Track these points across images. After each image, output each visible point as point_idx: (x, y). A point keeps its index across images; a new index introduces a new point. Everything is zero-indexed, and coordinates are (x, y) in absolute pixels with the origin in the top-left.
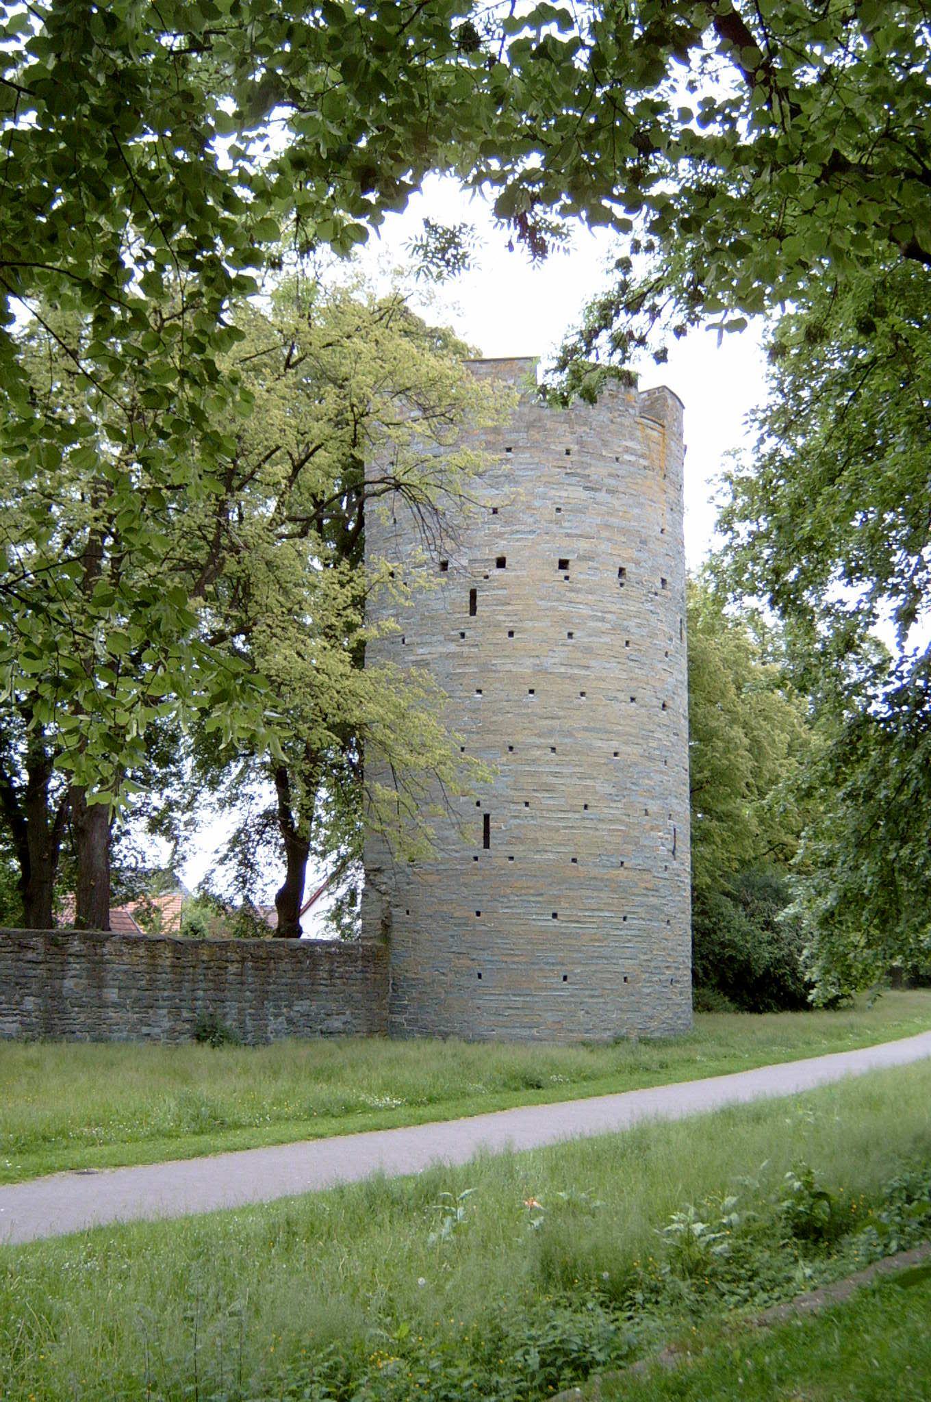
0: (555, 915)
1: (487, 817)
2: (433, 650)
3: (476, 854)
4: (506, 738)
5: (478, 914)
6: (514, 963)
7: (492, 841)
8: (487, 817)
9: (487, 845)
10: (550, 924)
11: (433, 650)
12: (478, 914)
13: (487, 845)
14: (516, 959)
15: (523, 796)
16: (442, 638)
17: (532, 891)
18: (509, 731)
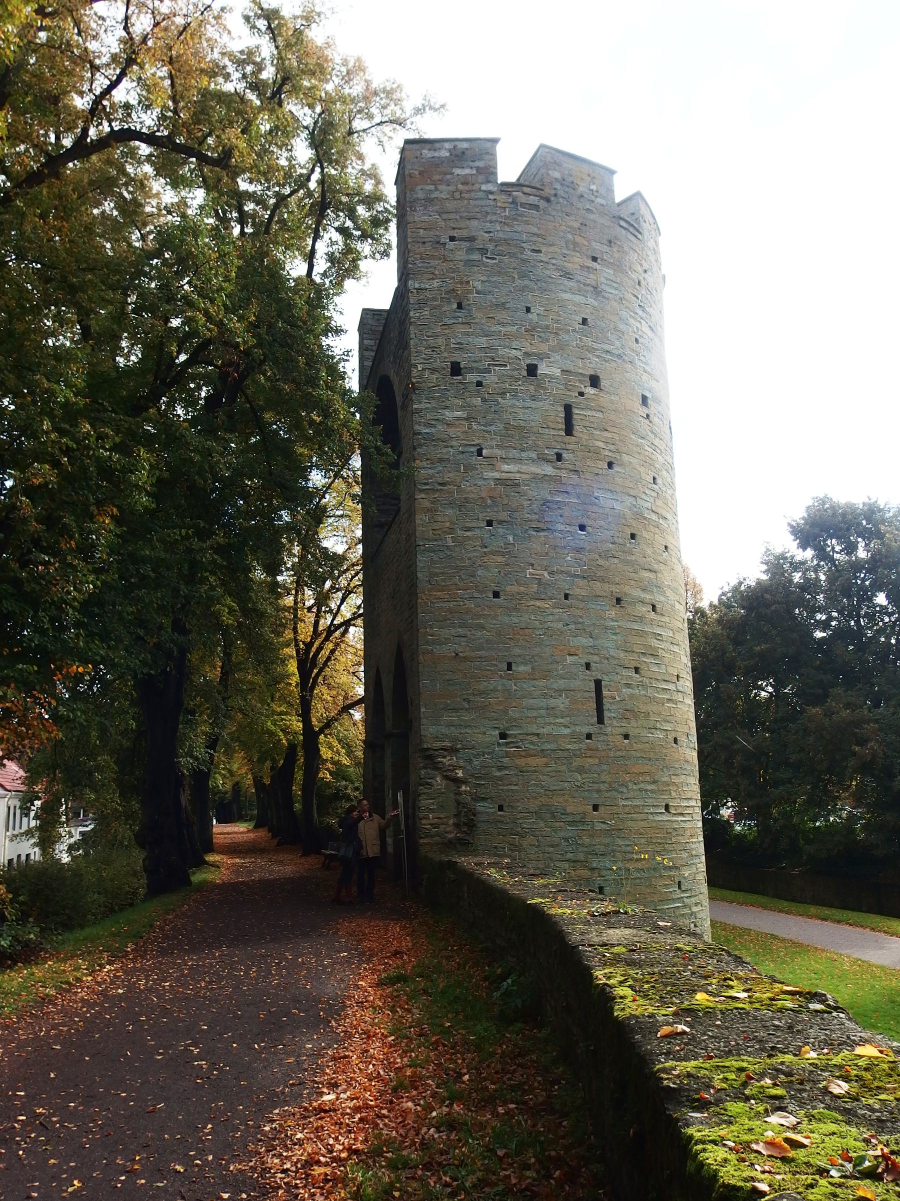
0: (667, 807)
1: (598, 684)
2: (524, 468)
3: (586, 730)
4: (614, 588)
5: (596, 808)
7: (606, 714)
8: (598, 684)
10: (665, 818)
11: (524, 468)
12: (596, 808)
13: (601, 720)
15: (631, 660)
16: (534, 455)
18: (617, 579)
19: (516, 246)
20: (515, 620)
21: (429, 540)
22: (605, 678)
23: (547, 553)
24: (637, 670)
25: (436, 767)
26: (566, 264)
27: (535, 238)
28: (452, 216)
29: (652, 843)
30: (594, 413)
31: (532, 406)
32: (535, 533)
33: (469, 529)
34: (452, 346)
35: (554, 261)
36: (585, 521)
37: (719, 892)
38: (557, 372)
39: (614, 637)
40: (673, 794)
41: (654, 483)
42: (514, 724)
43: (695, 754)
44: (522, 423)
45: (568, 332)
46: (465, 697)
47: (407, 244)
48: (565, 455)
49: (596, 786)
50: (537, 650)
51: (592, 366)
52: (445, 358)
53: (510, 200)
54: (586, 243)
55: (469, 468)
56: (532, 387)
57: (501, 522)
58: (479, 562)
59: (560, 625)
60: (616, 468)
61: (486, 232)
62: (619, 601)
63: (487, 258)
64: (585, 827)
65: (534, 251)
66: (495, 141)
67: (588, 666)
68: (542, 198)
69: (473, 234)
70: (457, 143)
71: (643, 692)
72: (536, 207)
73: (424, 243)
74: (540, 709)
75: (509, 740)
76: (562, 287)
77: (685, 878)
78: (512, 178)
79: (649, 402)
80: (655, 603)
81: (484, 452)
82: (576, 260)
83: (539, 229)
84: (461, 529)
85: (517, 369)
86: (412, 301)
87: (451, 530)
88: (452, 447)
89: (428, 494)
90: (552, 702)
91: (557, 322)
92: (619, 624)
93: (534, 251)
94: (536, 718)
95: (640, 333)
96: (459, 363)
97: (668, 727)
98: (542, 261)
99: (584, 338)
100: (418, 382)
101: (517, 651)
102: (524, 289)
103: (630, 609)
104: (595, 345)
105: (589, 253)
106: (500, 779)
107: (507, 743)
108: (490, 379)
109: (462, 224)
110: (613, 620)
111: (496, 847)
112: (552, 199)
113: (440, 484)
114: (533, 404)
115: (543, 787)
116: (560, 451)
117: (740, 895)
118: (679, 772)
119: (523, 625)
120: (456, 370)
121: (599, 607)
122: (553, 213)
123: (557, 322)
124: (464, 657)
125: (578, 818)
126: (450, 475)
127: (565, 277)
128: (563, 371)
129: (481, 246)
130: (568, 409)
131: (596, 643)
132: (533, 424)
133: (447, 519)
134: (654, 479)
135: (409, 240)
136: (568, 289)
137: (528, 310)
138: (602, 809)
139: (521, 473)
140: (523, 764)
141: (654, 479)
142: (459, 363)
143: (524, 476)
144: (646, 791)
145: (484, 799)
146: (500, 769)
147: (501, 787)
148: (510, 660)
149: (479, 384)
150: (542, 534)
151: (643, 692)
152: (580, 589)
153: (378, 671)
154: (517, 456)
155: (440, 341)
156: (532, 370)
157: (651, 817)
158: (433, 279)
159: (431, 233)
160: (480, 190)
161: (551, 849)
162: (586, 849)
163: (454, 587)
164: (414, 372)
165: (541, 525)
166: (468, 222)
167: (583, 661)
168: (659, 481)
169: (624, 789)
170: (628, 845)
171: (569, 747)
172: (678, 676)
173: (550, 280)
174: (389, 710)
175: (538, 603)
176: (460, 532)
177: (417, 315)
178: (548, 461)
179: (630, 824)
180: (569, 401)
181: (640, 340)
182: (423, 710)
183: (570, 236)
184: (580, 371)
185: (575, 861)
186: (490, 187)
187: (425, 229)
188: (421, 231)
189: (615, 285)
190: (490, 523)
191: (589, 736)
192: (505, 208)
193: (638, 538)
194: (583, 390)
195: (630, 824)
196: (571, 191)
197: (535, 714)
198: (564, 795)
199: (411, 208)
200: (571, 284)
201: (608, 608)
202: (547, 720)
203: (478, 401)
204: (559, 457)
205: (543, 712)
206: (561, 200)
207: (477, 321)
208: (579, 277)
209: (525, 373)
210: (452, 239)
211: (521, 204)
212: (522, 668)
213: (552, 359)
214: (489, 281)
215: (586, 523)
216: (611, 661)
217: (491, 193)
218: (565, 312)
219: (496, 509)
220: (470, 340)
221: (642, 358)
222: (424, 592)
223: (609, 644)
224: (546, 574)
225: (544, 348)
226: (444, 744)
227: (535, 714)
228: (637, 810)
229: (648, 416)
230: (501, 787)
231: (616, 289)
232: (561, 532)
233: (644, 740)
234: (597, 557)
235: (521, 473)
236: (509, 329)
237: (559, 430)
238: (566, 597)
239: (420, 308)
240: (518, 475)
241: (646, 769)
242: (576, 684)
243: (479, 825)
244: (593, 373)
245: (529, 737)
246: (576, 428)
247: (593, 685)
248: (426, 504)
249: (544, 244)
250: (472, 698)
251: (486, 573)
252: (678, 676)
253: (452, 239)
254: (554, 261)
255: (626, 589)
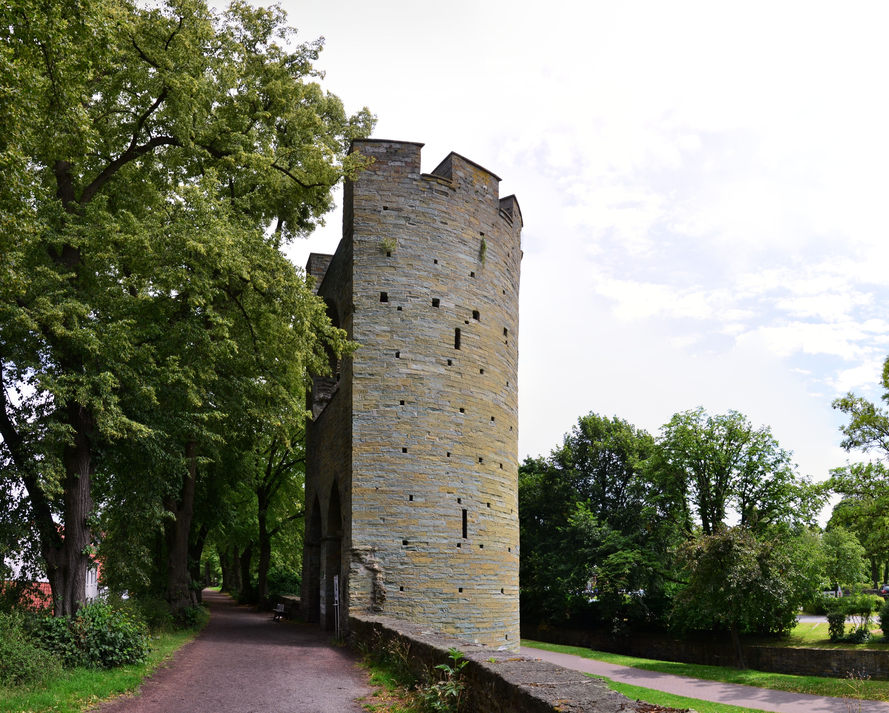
0: (502, 591)
1: (465, 512)
2: (426, 368)
3: (459, 541)
4: (478, 451)
5: (461, 590)
6: (483, 628)
7: (469, 532)
8: (465, 512)
9: (465, 536)
11: (426, 368)
12: (461, 590)
13: (465, 536)
14: (484, 625)
15: (486, 498)
16: (434, 360)
17: (492, 572)
18: (480, 446)
19: (430, 218)
20: (416, 468)
21: (361, 412)
22: (469, 509)
23: (439, 425)
24: (488, 505)
25: (361, 561)
26: (463, 234)
27: (443, 215)
28: (385, 193)
29: (493, 612)
30: (474, 336)
31: (435, 327)
32: (431, 411)
33: (388, 406)
34: (382, 281)
35: (455, 232)
36: (463, 406)
37: (525, 642)
38: (452, 306)
39: (476, 483)
40: (506, 583)
41: (507, 386)
42: (413, 535)
43: (518, 558)
44: (427, 338)
45: (461, 280)
46: (381, 516)
47: (352, 209)
48: (454, 362)
49: (462, 577)
50: (430, 488)
51: (475, 305)
52: (377, 289)
53: (428, 187)
54: (478, 223)
55: (390, 365)
56: (435, 314)
57: (409, 403)
58: (394, 429)
59: (443, 473)
60: (485, 374)
61: (410, 206)
62: (481, 460)
63: (409, 223)
64: (454, 602)
65: (442, 222)
66: (421, 145)
67: (459, 501)
68: (451, 188)
69: (401, 206)
70: (393, 144)
71: (491, 519)
72: (446, 194)
73: (365, 209)
74: (429, 526)
75: (408, 546)
76: (460, 250)
77: (510, 633)
78: (429, 172)
79: (508, 333)
80: (502, 463)
81: (401, 355)
82: (470, 233)
83: (447, 208)
84: (383, 405)
85: (426, 301)
86: (355, 249)
87: (377, 406)
88: (379, 350)
89: (361, 381)
90: (438, 523)
91: (455, 272)
92: (480, 475)
93: (442, 222)
94: (427, 532)
95: (506, 287)
96: (386, 294)
97: (506, 540)
98: (447, 230)
99: (471, 286)
100: (357, 305)
101: (417, 488)
102: (432, 248)
103: (487, 466)
104: (478, 291)
105: (479, 230)
106: (402, 570)
107: (407, 548)
108: (407, 306)
109: (394, 200)
110: (476, 472)
111: (397, 614)
112: (457, 190)
113: (370, 375)
114: (435, 326)
115: (429, 576)
116: (451, 359)
117: (707, 669)
118: (510, 569)
119: (421, 472)
120: (384, 298)
121: (468, 463)
122: (457, 199)
123: (455, 272)
124: (382, 491)
125: (449, 596)
126: (377, 369)
127: (462, 243)
128: (456, 305)
129: (406, 215)
130: (458, 331)
131: (465, 486)
132: (434, 339)
133: (374, 398)
134: (507, 383)
135: (354, 207)
136: (463, 251)
137: (436, 262)
138: (464, 591)
139: (424, 371)
140: (417, 562)
141: (507, 383)
142: (386, 294)
143: (426, 373)
144: (491, 580)
145: (391, 583)
146: (402, 564)
147: (403, 576)
148: (412, 494)
149: (400, 309)
150: (436, 412)
151: (491, 519)
152: (457, 450)
153: (316, 496)
154: (423, 359)
155: (374, 278)
156: (436, 303)
157: (493, 596)
158: (371, 235)
159: (370, 203)
160: (407, 178)
161: (432, 615)
162: (453, 616)
163: (377, 444)
164: (355, 298)
165: (436, 407)
166: (397, 198)
167: (456, 498)
168: (510, 385)
169: (478, 579)
170: (479, 614)
171: (446, 551)
172: (512, 510)
173: (451, 244)
174: (325, 523)
175: (431, 458)
176: (382, 408)
177: (359, 258)
178: (443, 365)
179: (480, 601)
180: (459, 326)
181: (506, 292)
182: (353, 524)
183: (467, 217)
184: (467, 307)
185: (446, 623)
186: (415, 176)
187: (366, 200)
188: (363, 201)
189: (494, 254)
190: (402, 403)
191: (459, 545)
192: (424, 191)
193: (495, 420)
194: (468, 320)
195: (480, 601)
196: (469, 186)
197: (426, 529)
198: (442, 581)
199: (356, 185)
200: (466, 248)
201: (473, 464)
202: (434, 534)
203: (398, 320)
204: (450, 363)
205: (431, 529)
206: (463, 192)
207: (400, 266)
208: (471, 245)
209: (431, 304)
210: (385, 208)
211: (436, 190)
212: (419, 500)
213: (449, 297)
214: (410, 240)
215: (464, 408)
216: (474, 498)
217: (415, 180)
218: (460, 267)
219: (407, 394)
220: (395, 278)
221: (506, 304)
222: (356, 446)
223: (473, 488)
224: (437, 439)
225: (444, 289)
226: (367, 547)
227: (426, 529)
228: (485, 592)
229: (506, 342)
230: (403, 576)
231: (494, 256)
232: (448, 412)
233: (492, 549)
234: (469, 430)
235: (424, 371)
236: (422, 273)
237: (450, 344)
238: (449, 455)
239: (361, 254)
240: (422, 373)
241: (492, 567)
242: (451, 512)
243: (387, 599)
244: (475, 310)
245: (421, 544)
246: (462, 344)
247: (461, 512)
248: (360, 387)
249: (449, 219)
250: (386, 518)
251: (398, 436)
252: (512, 510)
253: (385, 208)
254: (455, 232)
255: (486, 453)
